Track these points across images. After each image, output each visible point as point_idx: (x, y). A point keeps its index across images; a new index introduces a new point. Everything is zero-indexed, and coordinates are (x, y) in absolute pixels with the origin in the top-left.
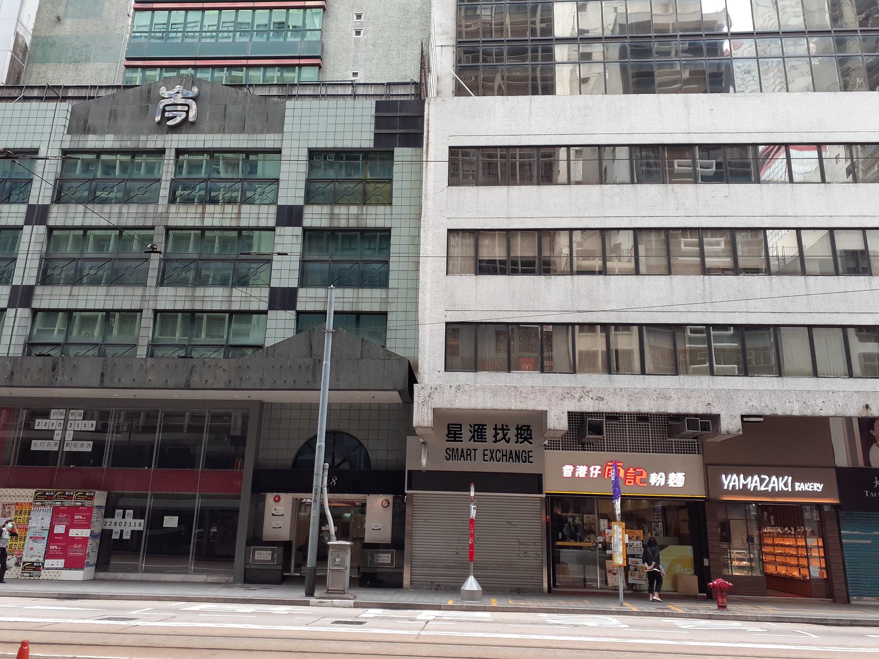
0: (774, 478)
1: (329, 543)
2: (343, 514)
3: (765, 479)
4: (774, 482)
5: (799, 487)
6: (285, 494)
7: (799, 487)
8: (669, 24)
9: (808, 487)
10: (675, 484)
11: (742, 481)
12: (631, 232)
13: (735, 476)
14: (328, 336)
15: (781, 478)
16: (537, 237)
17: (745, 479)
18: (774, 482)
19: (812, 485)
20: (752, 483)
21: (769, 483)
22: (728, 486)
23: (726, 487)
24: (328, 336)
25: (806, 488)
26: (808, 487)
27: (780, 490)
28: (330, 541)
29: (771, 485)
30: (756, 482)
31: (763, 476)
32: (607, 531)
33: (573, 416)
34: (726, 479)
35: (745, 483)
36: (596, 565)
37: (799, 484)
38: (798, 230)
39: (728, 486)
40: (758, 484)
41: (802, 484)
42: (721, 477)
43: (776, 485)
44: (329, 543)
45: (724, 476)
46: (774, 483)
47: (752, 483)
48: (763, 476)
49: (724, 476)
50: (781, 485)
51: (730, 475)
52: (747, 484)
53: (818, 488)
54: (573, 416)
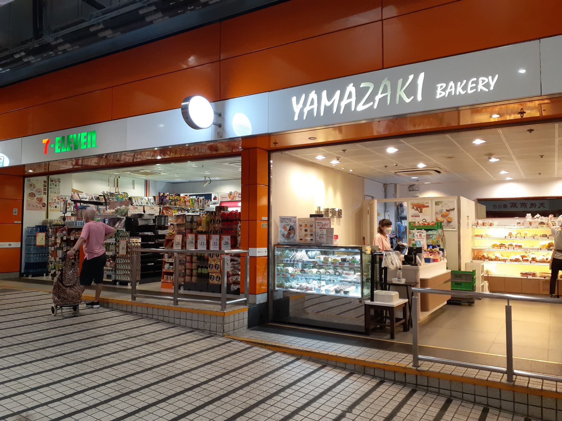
0: (452, 84)
2: (416, 165)
4: (451, 86)
5: (444, 90)
6: (260, 303)
7: (444, 90)
9: (464, 88)
11: (325, 102)
15: (459, 83)
17: (329, 97)
18: (451, 86)
21: (374, 93)
23: (296, 118)
25: (459, 90)
27: (458, 93)
29: (448, 91)
30: (350, 96)
31: (363, 85)
32: (166, 238)
33: (333, 229)
34: (298, 102)
35: (328, 104)
37: (444, 85)
38: (158, 308)
41: (452, 84)
42: (302, 95)
43: (453, 89)
45: (294, 99)
46: (451, 88)
48: (363, 85)
49: (294, 99)
50: (459, 90)
51: (304, 96)
52: (332, 105)
53: (487, 85)
54: (333, 229)
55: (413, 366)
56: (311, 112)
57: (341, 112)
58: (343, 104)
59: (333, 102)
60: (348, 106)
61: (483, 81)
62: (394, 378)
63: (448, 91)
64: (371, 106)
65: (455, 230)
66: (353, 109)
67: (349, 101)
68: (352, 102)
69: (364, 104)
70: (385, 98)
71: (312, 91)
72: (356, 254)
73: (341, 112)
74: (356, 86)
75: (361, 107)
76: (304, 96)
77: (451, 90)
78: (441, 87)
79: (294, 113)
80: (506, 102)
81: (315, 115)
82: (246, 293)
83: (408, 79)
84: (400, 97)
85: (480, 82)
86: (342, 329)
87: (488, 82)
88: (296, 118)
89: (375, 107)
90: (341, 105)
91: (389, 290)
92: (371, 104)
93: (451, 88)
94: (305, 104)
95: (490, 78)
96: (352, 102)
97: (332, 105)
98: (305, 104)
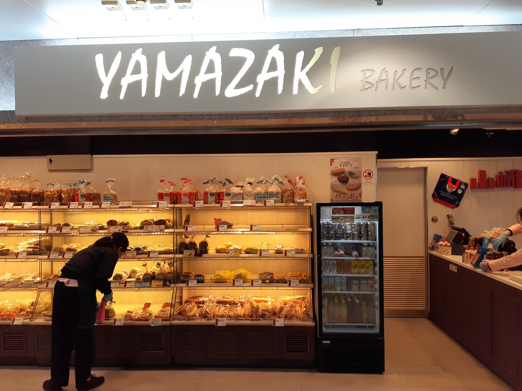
3: (241, 61)
18: (274, 63)
21: (256, 69)
22: (191, 85)
23: (104, 95)
29: (262, 78)
35: (170, 77)
39: (191, 85)
40: (218, 75)
43: (280, 73)
52: (179, 79)
56: (135, 86)
57: (196, 95)
58: (199, 81)
59: (181, 72)
60: (209, 85)
64: (249, 92)
66: (218, 92)
67: (272, 75)
69: (238, 87)
70: (273, 82)
72: (328, 227)
73: (196, 95)
75: (231, 92)
79: (101, 85)
80: (41, 275)
81: (144, 94)
82: (61, 280)
88: (104, 95)
89: (258, 94)
90: (195, 82)
92: (250, 87)
93: (273, 67)
94: (195, 71)
97: (179, 79)
98: (121, 73)
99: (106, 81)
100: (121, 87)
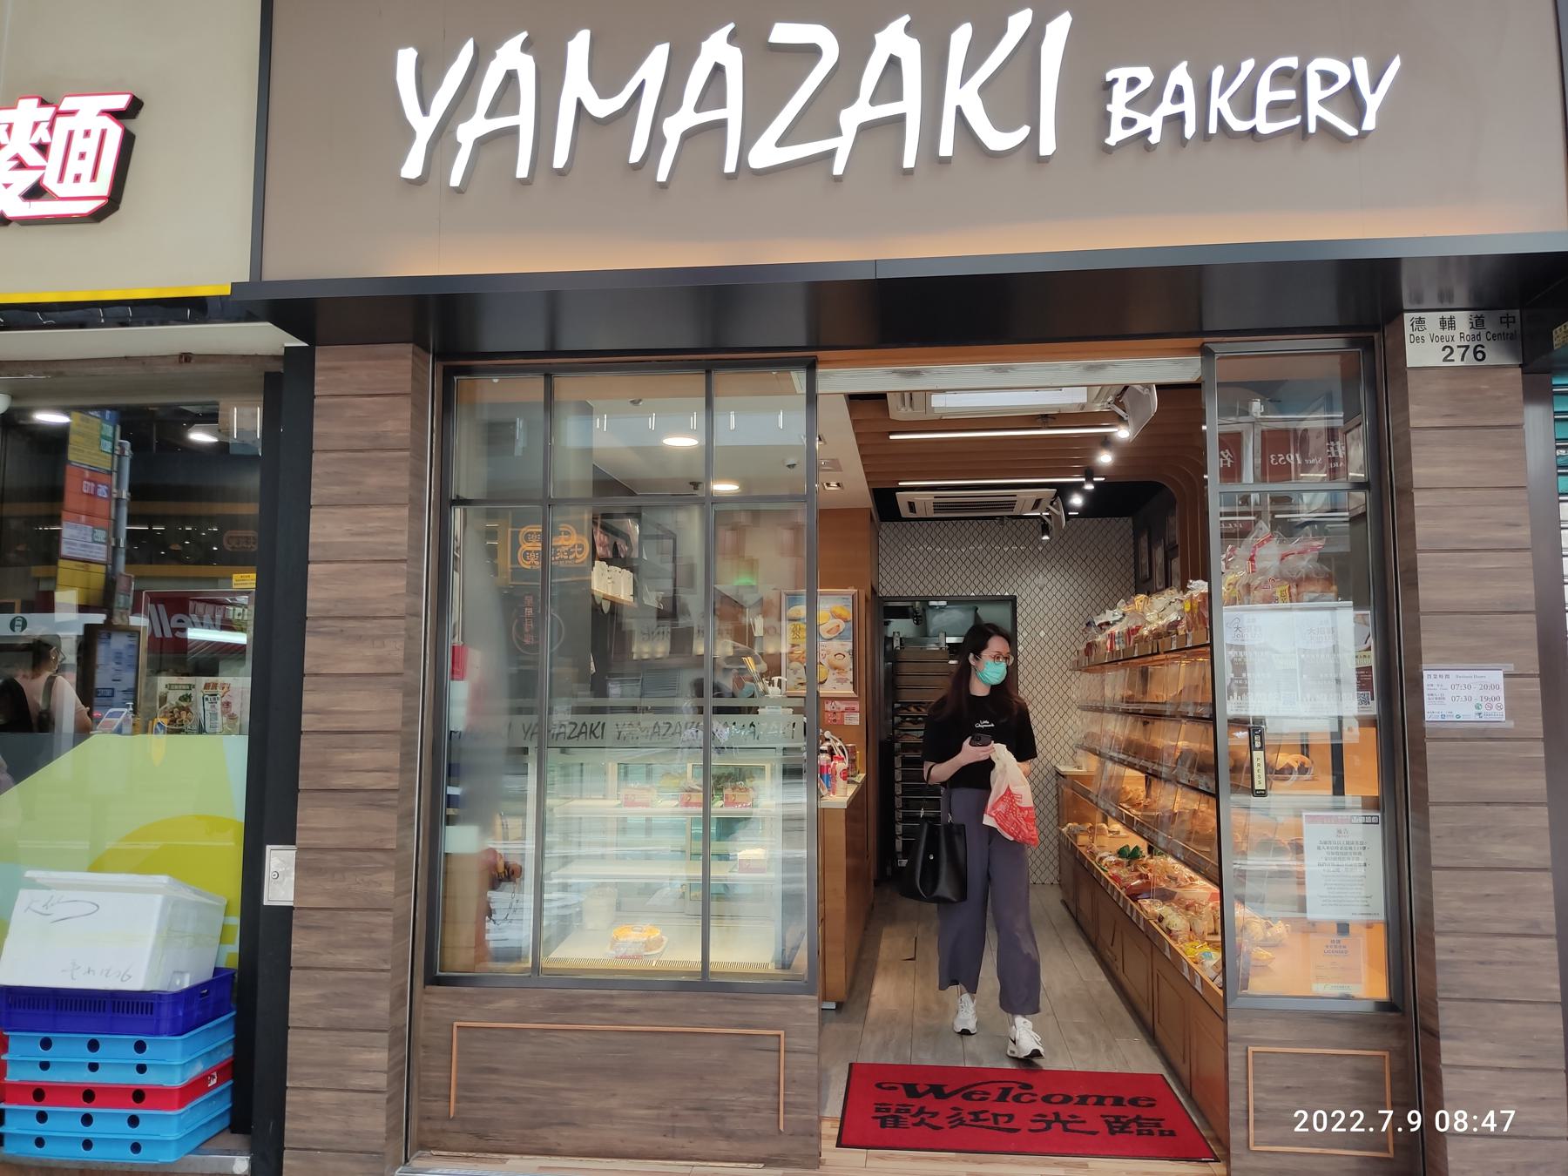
1: (1325, 475)
7: (1147, 101)
8: (140, 627)
9: (1245, 103)
10: (36, 192)
12: (222, 945)
13: (512, 56)
14: (348, 769)
16: (319, 1001)
17: (606, 77)
19: (1282, 77)
20: (669, 101)
21: (842, 86)
22: (656, 139)
24: (348, 769)
26: (1245, 103)
28: (1324, 477)
31: (784, 33)
35: (601, 108)
36: (429, 353)
37: (1146, 76)
43: (1189, 107)
44: (1325, 475)
47: (669, 101)
48: (784, 33)
55: (972, 988)
61: (1328, 79)
62: (699, 958)
63: (1167, 108)
65: (1429, 672)
68: (1255, 126)
71: (468, 39)
74: (751, 39)
76: (467, 52)
77: (1177, 109)
78: (1133, 82)
83: (1002, 30)
84: (1221, 120)
85: (1313, 81)
86: (535, 827)
87: (1353, 84)
91: (1304, 878)
95: (1361, 65)
96: (1255, 126)
99: (424, 127)
100: (457, 146)
